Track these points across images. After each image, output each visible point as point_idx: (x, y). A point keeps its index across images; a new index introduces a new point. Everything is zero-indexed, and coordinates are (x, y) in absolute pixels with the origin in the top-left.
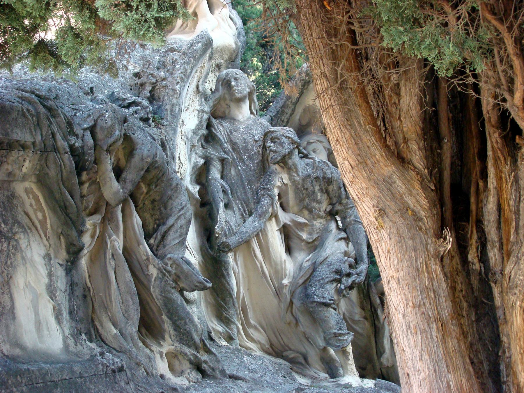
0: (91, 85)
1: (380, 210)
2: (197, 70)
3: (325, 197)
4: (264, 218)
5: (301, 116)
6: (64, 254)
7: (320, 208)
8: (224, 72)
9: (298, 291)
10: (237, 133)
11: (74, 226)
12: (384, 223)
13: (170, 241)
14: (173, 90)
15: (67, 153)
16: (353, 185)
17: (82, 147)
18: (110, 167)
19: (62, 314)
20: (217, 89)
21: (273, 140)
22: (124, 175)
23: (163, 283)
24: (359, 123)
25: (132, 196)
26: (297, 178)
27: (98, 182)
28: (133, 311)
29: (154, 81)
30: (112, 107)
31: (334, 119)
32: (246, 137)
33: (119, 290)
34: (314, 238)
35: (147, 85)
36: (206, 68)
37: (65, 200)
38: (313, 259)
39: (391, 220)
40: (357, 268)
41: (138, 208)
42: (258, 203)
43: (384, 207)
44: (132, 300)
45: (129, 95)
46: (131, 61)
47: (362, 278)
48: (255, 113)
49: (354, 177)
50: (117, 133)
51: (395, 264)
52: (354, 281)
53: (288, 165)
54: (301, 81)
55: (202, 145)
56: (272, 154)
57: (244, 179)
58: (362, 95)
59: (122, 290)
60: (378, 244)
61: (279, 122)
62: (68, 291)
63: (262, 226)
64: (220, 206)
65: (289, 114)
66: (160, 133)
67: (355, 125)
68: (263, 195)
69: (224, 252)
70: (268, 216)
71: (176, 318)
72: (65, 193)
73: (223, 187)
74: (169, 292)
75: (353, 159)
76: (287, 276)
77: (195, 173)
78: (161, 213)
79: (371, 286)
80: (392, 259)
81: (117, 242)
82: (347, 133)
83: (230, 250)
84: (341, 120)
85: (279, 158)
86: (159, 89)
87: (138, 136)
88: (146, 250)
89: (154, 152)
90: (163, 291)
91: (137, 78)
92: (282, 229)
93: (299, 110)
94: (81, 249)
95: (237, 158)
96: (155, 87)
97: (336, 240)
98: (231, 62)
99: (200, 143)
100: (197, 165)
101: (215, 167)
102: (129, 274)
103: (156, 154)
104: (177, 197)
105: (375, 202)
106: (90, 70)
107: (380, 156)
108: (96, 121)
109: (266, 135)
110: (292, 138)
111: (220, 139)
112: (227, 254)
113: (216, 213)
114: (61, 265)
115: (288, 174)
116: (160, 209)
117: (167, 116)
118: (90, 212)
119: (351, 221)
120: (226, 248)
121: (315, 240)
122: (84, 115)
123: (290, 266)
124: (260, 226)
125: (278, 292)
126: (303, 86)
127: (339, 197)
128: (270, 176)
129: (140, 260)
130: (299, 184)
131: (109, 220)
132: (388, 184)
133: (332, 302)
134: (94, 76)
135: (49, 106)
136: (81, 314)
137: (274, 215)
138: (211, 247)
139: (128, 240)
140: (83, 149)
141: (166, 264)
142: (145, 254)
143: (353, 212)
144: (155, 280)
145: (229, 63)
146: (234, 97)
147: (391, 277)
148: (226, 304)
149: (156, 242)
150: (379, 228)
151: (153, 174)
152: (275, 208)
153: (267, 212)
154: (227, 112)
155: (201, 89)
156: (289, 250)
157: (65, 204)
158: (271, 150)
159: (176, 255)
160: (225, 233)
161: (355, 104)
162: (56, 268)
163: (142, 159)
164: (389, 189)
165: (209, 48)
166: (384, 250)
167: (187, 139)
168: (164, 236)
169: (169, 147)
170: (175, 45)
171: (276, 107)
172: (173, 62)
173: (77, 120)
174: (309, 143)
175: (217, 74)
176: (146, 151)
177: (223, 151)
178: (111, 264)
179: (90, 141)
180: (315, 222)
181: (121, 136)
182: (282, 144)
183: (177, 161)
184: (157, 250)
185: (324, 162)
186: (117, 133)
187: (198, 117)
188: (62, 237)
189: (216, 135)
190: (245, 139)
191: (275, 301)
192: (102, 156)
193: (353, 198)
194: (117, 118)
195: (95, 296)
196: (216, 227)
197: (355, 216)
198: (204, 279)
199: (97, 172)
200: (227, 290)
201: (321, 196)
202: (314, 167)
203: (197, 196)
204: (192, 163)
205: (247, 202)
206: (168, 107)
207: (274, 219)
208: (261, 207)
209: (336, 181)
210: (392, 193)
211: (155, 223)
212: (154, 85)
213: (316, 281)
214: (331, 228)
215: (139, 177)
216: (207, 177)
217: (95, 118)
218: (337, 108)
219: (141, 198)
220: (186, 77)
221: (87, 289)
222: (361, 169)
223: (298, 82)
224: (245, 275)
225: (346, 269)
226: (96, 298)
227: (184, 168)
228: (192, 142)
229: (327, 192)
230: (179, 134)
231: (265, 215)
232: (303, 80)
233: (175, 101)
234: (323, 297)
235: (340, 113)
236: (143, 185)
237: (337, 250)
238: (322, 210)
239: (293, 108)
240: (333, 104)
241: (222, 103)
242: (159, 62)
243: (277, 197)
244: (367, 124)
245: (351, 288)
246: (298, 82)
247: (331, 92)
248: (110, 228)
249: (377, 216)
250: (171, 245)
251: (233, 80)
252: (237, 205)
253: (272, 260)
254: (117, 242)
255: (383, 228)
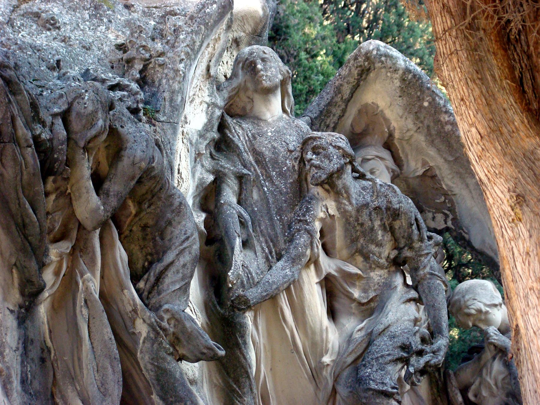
0: (57, 57)
1: (518, 196)
2: (209, 44)
3: (388, 237)
4: (298, 264)
5: (354, 120)
6: (16, 296)
7: (380, 254)
8: (247, 50)
9: (346, 373)
10: (264, 139)
11: (34, 254)
12: (523, 214)
13: (168, 286)
14: (174, 71)
15: (30, 147)
16: (482, 161)
17: (51, 140)
18: (87, 173)
19: (11, 383)
20: (234, 74)
21: (316, 151)
22: (106, 185)
23: (155, 346)
24: (493, 77)
25: (116, 218)
26: (349, 208)
27: (70, 194)
28: (112, 383)
29: (147, 56)
30: (94, 86)
31: (459, 70)
32: (276, 145)
33: (94, 352)
34: (371, 297)
35: (136, 61)
36: (221, 42)
37: (24, 215)
38: (368, 328)
39: (532, 211)
40: (432, 344)
41: (123, 236)
42: (291, 241)
43: (523, 193)
44: (112, 367)
45: (110, 75)
46: (113, 27)
47: (440, 358)
48: (289, 111)
49: (483, 149)
50: (100, 123)
51: (537, 272)
52: (428, 362)
53: (337, 187)
54: (357, 67)
55: (211, 154)
56: (314, 171)
57: (272, 206)
58: (498, 39)
59: (99, 353)
60: (512, 243)
61: (322, 127)
62: (20, 349)
63: (296, 275)
64: (235, 242)
65: (337, 115)
66: (155, 132)
67: (487, 79)
68: (299, 230)
69: (239, 310)
70: (304, 260)
71: (173, 399)
72: (25, 204)
73: (240, 216)
74: (164, 359)
75: (483, 126)
76: (330, 352)
77: (199, 194)
78: (155, 246)
79: (449, 375)
80: (532, 264)
81: (91, 282)
82: (477, 89)
83: (249, 308)
84: (469, 72)
85: (324, 177)
86: (154, 68)
87: (128, 128)
88: (133, 296)
89: (151, 154)
90: (156, 359)
91: (122, 52)
92: (324, 283)
93: (352, 111)
94: (41, 289)
95: (262, 175)
96: (148, 64)
97: (402, 300)
98: (255, 36)
99: (208, 151)
100: (204, 183)
101: (229, 186)
102: (109, 330)
103: (153, 158)
104: (179, 223)
105: (511, 185)
106: (52, 38)
107: (520, 123)
108: (70, 105)
109: (305, 142)
110: (343, 149)
111: (238, 147)
112: (244, 313)
113: (230, 254)
114: (12, 311)
115: (335, 201)
116: (154, 239)
117: (165, 107)
118: (54, 237)
119: (425, 275)
120: (243, 304)
121: (371, 300)
122: (53, 95)
123: (333, 337)
124: (293, 275)
125: (315, 375)
126: (360, 75)
127: (410, 238)
128: (310, 203)
129: (123, 312)
130: (351, 217)
131: (81, 251)
132: (529, 161)
133: (395, 391)
134: (59, 45)
135: (8, 77)
136: (36, 385)
137: (313, 260)
138: (221, 303)
139: (106, 281)
140: (52, 143)
141: (162, 319)
142: (131, 302)
143: (429, 261)
144: (144, 342)
145: (253, 38)
146: (259, 87)
147: (530, 289)
148: (239, 387)
149: (147, 286)
150: (516, 221)
151: (147, 187)
152: (316, 250)
153: (303, 255)
154: (248, 107)
155: (212, 72)
156: (332, 313)
157: (23, 221)
158: (312, 165)
159: (174, 306)
160: (242, 282)
161: (489, 50)
162: (4, 315)
163: (133, 164)
164: (531, 168)
165: (227, 13)
166: (522, 250)
167: (191, 143)
168: (159, 278)
169: (166, 153)
170: (176, 7)
171: (318, 105)
172: (175, 30)
173: (43, 102)
174: (365, 160)
175: (235, 54)
176: (139, 151)
177: (242, 164)
178: (82, 314)
179: (62, 133)
180: (372, 274)
181: (105, 127)
182: (328, 157)
183: (176, 174)
184: (148, 298)
185: (389, 186)
186: (100, 123)
187: (207, 113)
188: (14, 271)
189: (233, 141)
190: (274, 148)
191: (311, 388)
192: (77, 156)
193: (481, 180)
194: (101, 102)
195: (57, 361)
196: (229, 274)
197: (431, 267)
198: (214, 344)
199: (67, 179)
200: (243, 367)
201: (383, 236)
202: (373, 192)
203: (202, 227)
204: (196, 180)
205: (275, 239)
206: (167, 95)
207: (312, 267)
208: (295, 247)
209: (405, 214)
210: (535, 174)
211: (147, 260)
212: (146, 63)
213: (372, 359)
214: (396, 284)
215: (128, 190)
216: (217, 201)
217: (70, 100)
218: (463, 55)
219: (127, 223)
220: (193, 52)
221: (46, 351)
222: (493, 139)
223: (353, 69)
224: (267, 347)
225: (416, 343)
226: (59, 362)
227: (185, 185)
228: (197, 149)
229: (392, 230)
230: (180, 136)
231: (301, 260)
232: (361, 66)
233: (176, 86)
234: (383, 383)
235: (468, 63)
236: (130, 203)
237: (404, 316)
238: (383, 256)
239: (343, 107)
240: (459, 48)
241: (242, 95)
242: (154, 29)
243: (319, 233)
244: (503, 78)
245: (422, 372)
246: (353, 69)
247: (457, 34)
248: (82, 262)
249: (513, 204)
250: (168, 292)
251: (259, 61)
252: (261, 243)
253: (308, 326)
254: (91, 282)
255: (520, 220)
